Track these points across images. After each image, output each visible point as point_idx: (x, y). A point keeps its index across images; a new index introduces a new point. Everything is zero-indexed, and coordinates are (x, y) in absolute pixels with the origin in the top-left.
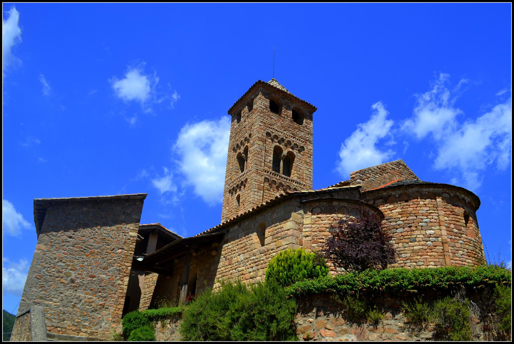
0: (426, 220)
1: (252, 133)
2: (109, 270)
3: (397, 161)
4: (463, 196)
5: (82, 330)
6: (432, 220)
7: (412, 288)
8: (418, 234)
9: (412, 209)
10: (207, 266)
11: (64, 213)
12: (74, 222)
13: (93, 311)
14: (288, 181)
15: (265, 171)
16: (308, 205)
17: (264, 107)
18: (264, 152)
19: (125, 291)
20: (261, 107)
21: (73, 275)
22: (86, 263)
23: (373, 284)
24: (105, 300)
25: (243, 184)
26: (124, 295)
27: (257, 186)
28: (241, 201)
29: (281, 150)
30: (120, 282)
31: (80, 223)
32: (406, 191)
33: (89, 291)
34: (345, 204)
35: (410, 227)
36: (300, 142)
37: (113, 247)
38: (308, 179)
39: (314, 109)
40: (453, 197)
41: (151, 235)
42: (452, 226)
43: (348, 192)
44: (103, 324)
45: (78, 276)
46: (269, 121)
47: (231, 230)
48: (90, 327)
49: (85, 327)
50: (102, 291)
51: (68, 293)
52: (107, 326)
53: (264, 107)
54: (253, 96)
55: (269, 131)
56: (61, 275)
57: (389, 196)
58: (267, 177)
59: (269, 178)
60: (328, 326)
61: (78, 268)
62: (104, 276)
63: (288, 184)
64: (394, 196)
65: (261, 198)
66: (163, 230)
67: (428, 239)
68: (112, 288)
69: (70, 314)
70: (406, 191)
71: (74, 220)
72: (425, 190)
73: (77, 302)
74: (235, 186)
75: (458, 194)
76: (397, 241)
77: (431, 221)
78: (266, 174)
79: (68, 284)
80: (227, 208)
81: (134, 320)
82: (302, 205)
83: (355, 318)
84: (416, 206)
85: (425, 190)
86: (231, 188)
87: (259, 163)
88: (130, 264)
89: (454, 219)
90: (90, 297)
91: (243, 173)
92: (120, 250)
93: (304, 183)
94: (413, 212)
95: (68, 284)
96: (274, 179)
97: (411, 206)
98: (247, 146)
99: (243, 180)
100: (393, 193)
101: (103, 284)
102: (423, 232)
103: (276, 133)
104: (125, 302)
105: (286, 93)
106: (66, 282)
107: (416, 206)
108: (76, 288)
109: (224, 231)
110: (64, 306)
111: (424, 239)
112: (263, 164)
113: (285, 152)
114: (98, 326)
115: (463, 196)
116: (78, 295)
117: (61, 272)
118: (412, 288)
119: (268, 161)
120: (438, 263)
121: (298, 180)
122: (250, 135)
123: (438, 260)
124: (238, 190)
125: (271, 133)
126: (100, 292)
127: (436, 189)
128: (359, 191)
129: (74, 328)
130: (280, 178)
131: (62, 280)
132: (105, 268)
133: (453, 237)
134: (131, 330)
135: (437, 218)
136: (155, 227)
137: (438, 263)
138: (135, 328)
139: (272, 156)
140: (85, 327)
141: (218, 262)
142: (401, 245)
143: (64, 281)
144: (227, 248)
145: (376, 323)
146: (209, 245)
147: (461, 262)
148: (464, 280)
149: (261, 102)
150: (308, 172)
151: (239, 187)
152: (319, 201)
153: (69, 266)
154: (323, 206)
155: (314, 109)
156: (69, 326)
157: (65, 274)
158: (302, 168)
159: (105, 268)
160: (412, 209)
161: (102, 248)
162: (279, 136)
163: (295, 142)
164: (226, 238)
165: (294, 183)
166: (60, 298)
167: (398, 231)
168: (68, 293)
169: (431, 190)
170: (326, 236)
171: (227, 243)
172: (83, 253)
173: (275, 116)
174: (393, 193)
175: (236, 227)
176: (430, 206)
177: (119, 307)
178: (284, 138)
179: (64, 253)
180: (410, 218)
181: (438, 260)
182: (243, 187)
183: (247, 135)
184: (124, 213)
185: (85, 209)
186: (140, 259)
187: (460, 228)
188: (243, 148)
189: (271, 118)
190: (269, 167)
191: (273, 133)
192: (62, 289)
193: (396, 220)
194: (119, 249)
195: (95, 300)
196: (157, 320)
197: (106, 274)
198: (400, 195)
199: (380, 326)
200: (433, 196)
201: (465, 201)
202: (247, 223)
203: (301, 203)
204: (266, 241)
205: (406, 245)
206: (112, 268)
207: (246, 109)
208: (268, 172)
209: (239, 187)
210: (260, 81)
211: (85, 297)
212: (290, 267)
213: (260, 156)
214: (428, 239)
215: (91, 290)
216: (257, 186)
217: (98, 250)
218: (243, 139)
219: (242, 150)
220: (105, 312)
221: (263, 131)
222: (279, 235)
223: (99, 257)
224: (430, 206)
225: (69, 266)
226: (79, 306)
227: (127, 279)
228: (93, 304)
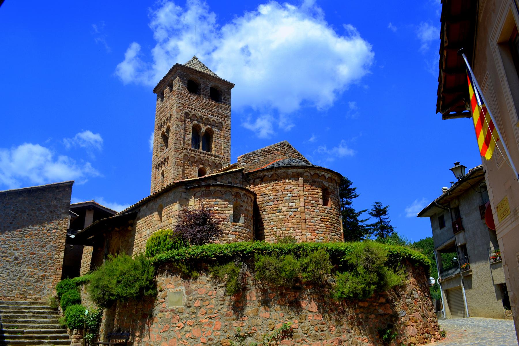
0: (290, 195)
2: (47, 247)
3: (282, 142)
4: (323, 173)
5: (28, 297)
6: (294, 195)
7: (214, 257)
8: (283, 206)
9: (279, 186)
10: (126, 238)
11: (3, 203)
12: (13, 210)
13: (36, 282)
14: (207, 156)
15: (185, 149)
16: (192, 190)
17: (182, 89)
18: (183, 131)
19: (62, 263)
20: (179, 89)
21: (16, 254)
22: (26, 244)
23: (193, 255)
24: (46, 272)
25: (166, 160)
26: (61, 266)
27: (177, 163)
28: (165, 176)
29: (200, 128)
30: (56, 256)
31: (17, 211)
32: (276, 172)
33: (31, 266)
34: (219, 188)
36: (218, 118)
37: (48, 228)
38: (226, 151)
40: (314, 174)
42: (310, 198)
43: (231, 175)
44: (45, 291)
45: (21, 255)
46: (188, 101)
47: (142, 209)
48: (35, 294)
49: (30, 294)
50: (42, 265)
51: (13, 269)
52: (49, 292)
53: (182, 89)
54: (173, 78)
55: (188, 111)
56: (6, 254)
57: (265, 176)
58: (186, 153)
60: (171, 282)
61: (20, 248)
62: (43, 252)
63: (206, 158)
64: (268, 176)
65: (181, 173)
66: (96, 206)
67: (290, 210)
68: (50, 262)
69: (17, 285)
70: (276, 172)
71: (12, 208)
72: (290, 171)
73: (22, 275)
74: (160, 162)
75: (318, 172)
76: (268, 212)
78: (185, 151)
79: (12, 262)
80: (155, 182)
81: (65, 286)
82: (187, 190)
83: (186, 277)
84: (282, 184)
85: (290, 171)
86: (157, 164)
87: (178, 142)
88: (64, 241)
89: (312, 193)
90: (32, 270)
92: (54, 231)
93: (222, 156)
95: (12, 262)
96: (193, 155)
97: (279, 185)
98: (169, 125)
99: (166, 157)
100: (267, 174)
101: (42, 259)
102: (287, 205)
103: (195, 112)
104: (62, 272)
105: (204, 73)
106: (11, 260)
107: (282, 184)
108: (20, 264)
109: (137, 210)
110: (11, 279)
111: (287, 210)
112: (182, 142)
113: (204, 129)
114: (42, 293)
115: (323, 173)
116: (22, 269)
117: (6, 253)
118: (214, 257)
119: (187, 139)
120: (296, 228)
121: (217, 154)
122: (171, 115)
123: (296, 226)
124: (163, 166)
125: (189, 113)
126: (40, 266)
127: (299, 170)
128: (243, 173)
129: (21, 296)
131: (8, 259)
132: (43, 246)
133: (310, 207)
134: (62, 294)
135: (298, 192)
136: (90, 204)
137: (296, 228)
138: (65, 292)
139: (191, 134)
140: (30, 294)
141: (135, 235)
142: (270, 215)
143: (9, 260)
144: (140, 223)
145: (196, 278)
146: (128, 221)
147: (314, 227)
148: (243, 251)
149: (177, 85)
150: (226, 146)
151: (163, 163)
152: (200, 187)
153: (12, 246)
154: (203, 191)
156: (17, 295)
157: (9, 253)
158: (221, 142)
159: (43, 246)
160: (279, 186)
161: (39, 229)
162: (197, 115)
163: (213, 119)
164: (138, 216)
165: (212, 157)
166: (7, 273)
167: (269, 204)
168: (13, 269)
169: (295, 170)
170: (174, 225)
171: (144, 217)
172: (22, 235)
173: (193, 97)
174: (267, 174)
175: (145, 207)
177: (57, 276)
178: (203, 116)
179: (7, 237)
180: (278, 193)
181: (296, 226)
182: (166, 163)
183: (168, 115)
184: (56, 199)
185: (21, 198)
186: (73, 236)
187: (317, 199)
188: (166, 127)
189: (189, 99)
190: (189, 145)
191: (191, 112)
192: (8, 266)
193: (269, 195)
194: (54, 229)
195: (37, 273)
196: (82, 285)
197: (44, 251)
198: (272, 175)
199: (198, 281)
200: (296, 177)
201: (325, 177)
202: (151, 204)
203: (186, 189)
204: (164, 219)
205: (274, 215)
206: (49, 246)
207: (167, 89)
208: (187, 149)
209: (163, 163)
210: (177, 64)
211: (28, 271)
212: (159, 243)
213: (179, 135)
214: (290, 210)
215: (33, 265)
216: (177, 163)
217: (36, 232)
218: (165, 119)
219: (164, 129)
220: (46, 281)
221: (181, 112)
222: (170, 215)
223: (37, 237)
225: (12, 246)
226: (23, 278)
227: (62, 254)
228: (35, 276)
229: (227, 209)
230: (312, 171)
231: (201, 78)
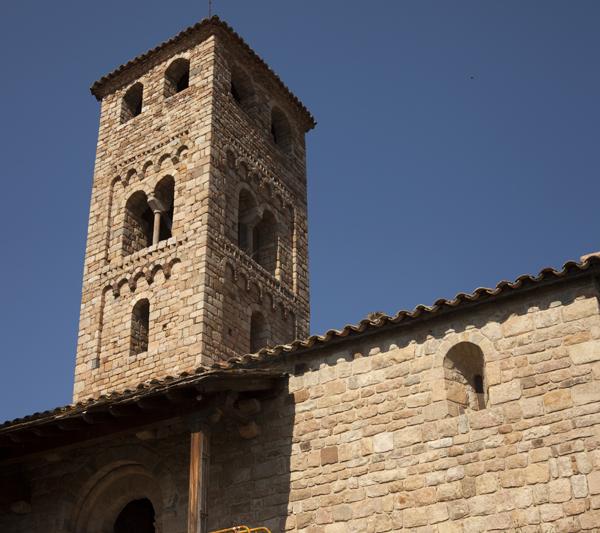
58: (231, 262)
59: (234, 266)
96: (244, 271)
208: (232, 251)
210: (216, 19)
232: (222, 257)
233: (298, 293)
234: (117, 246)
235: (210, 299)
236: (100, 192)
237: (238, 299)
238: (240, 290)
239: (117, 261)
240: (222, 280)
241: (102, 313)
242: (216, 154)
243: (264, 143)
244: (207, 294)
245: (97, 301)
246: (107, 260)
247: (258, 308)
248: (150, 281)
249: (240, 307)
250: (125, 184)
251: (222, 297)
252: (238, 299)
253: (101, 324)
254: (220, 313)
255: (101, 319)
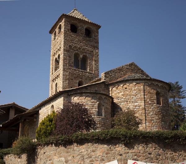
1: (61, 46)
9: (128, 93)
10: (33, 126)
14: (84, 73)
17: (67, 30)
28: (57, 87)
35: (127, 102)
39: (99, 27)
40: (151, 84)
41: (11, 108)
43: (97, 85)
53: (67, 30)
55: (71, 45)
58: (71, 72)
59: (72, 73)
77: (137, 98)
78: (69, 70)
82: (69, 96)
86: (53, 79)
91: (53, 75)
94: (129, 94)
96: (75, 73)
99: (58, 75)
102: (133, 104)
115: (157, 83)
125: (72, 46)
130: (79, 72)
135: (140, 96)
139: (73, 59)
147: (151, 118)
155: (99, 27)
160: (128, 93)
173: (73, 35)
176: (137, 90)
180: (127, 97)
183: (59, 48)
189: (72, 36)
191: (73, 45)
201: (158, 86)
208: (71, 69)
210: (63, 14)
224: (137, 90)
229: (94, 107)
230: (150, 82)
231: (79, 23)
232: (67, 72)
233: (94, 72)
234: (54, 70)
235: (64, 82)
236: (51, 58)
237: (74, 79)
238: (74, 77)
239: (54, 73)
240: (68, 77)
241: (52, 86)
242: (65, 48)
243: (82, 38)
244: (63, 81)
245: (51, 83)
246: (52, 74)
247: (80, 80)
248: (57, 79)
249: (74, 81)
250: (55, 56)
251: (68, 81)
252: (74, 79)
253: (52, 88)
254: (67, 84)
255: (52, 87)
